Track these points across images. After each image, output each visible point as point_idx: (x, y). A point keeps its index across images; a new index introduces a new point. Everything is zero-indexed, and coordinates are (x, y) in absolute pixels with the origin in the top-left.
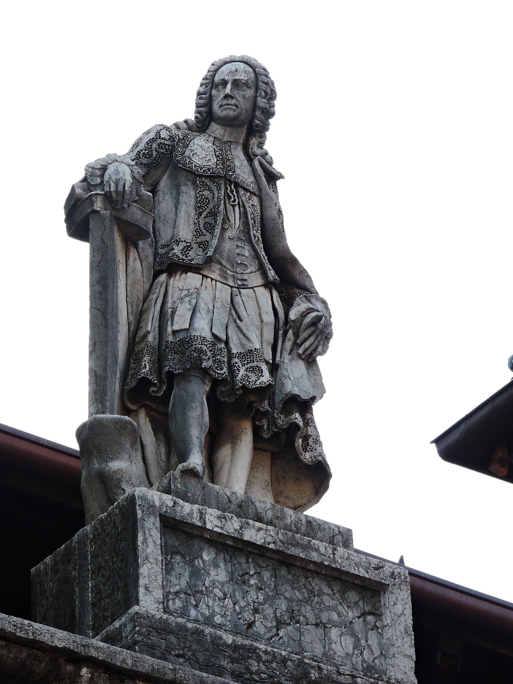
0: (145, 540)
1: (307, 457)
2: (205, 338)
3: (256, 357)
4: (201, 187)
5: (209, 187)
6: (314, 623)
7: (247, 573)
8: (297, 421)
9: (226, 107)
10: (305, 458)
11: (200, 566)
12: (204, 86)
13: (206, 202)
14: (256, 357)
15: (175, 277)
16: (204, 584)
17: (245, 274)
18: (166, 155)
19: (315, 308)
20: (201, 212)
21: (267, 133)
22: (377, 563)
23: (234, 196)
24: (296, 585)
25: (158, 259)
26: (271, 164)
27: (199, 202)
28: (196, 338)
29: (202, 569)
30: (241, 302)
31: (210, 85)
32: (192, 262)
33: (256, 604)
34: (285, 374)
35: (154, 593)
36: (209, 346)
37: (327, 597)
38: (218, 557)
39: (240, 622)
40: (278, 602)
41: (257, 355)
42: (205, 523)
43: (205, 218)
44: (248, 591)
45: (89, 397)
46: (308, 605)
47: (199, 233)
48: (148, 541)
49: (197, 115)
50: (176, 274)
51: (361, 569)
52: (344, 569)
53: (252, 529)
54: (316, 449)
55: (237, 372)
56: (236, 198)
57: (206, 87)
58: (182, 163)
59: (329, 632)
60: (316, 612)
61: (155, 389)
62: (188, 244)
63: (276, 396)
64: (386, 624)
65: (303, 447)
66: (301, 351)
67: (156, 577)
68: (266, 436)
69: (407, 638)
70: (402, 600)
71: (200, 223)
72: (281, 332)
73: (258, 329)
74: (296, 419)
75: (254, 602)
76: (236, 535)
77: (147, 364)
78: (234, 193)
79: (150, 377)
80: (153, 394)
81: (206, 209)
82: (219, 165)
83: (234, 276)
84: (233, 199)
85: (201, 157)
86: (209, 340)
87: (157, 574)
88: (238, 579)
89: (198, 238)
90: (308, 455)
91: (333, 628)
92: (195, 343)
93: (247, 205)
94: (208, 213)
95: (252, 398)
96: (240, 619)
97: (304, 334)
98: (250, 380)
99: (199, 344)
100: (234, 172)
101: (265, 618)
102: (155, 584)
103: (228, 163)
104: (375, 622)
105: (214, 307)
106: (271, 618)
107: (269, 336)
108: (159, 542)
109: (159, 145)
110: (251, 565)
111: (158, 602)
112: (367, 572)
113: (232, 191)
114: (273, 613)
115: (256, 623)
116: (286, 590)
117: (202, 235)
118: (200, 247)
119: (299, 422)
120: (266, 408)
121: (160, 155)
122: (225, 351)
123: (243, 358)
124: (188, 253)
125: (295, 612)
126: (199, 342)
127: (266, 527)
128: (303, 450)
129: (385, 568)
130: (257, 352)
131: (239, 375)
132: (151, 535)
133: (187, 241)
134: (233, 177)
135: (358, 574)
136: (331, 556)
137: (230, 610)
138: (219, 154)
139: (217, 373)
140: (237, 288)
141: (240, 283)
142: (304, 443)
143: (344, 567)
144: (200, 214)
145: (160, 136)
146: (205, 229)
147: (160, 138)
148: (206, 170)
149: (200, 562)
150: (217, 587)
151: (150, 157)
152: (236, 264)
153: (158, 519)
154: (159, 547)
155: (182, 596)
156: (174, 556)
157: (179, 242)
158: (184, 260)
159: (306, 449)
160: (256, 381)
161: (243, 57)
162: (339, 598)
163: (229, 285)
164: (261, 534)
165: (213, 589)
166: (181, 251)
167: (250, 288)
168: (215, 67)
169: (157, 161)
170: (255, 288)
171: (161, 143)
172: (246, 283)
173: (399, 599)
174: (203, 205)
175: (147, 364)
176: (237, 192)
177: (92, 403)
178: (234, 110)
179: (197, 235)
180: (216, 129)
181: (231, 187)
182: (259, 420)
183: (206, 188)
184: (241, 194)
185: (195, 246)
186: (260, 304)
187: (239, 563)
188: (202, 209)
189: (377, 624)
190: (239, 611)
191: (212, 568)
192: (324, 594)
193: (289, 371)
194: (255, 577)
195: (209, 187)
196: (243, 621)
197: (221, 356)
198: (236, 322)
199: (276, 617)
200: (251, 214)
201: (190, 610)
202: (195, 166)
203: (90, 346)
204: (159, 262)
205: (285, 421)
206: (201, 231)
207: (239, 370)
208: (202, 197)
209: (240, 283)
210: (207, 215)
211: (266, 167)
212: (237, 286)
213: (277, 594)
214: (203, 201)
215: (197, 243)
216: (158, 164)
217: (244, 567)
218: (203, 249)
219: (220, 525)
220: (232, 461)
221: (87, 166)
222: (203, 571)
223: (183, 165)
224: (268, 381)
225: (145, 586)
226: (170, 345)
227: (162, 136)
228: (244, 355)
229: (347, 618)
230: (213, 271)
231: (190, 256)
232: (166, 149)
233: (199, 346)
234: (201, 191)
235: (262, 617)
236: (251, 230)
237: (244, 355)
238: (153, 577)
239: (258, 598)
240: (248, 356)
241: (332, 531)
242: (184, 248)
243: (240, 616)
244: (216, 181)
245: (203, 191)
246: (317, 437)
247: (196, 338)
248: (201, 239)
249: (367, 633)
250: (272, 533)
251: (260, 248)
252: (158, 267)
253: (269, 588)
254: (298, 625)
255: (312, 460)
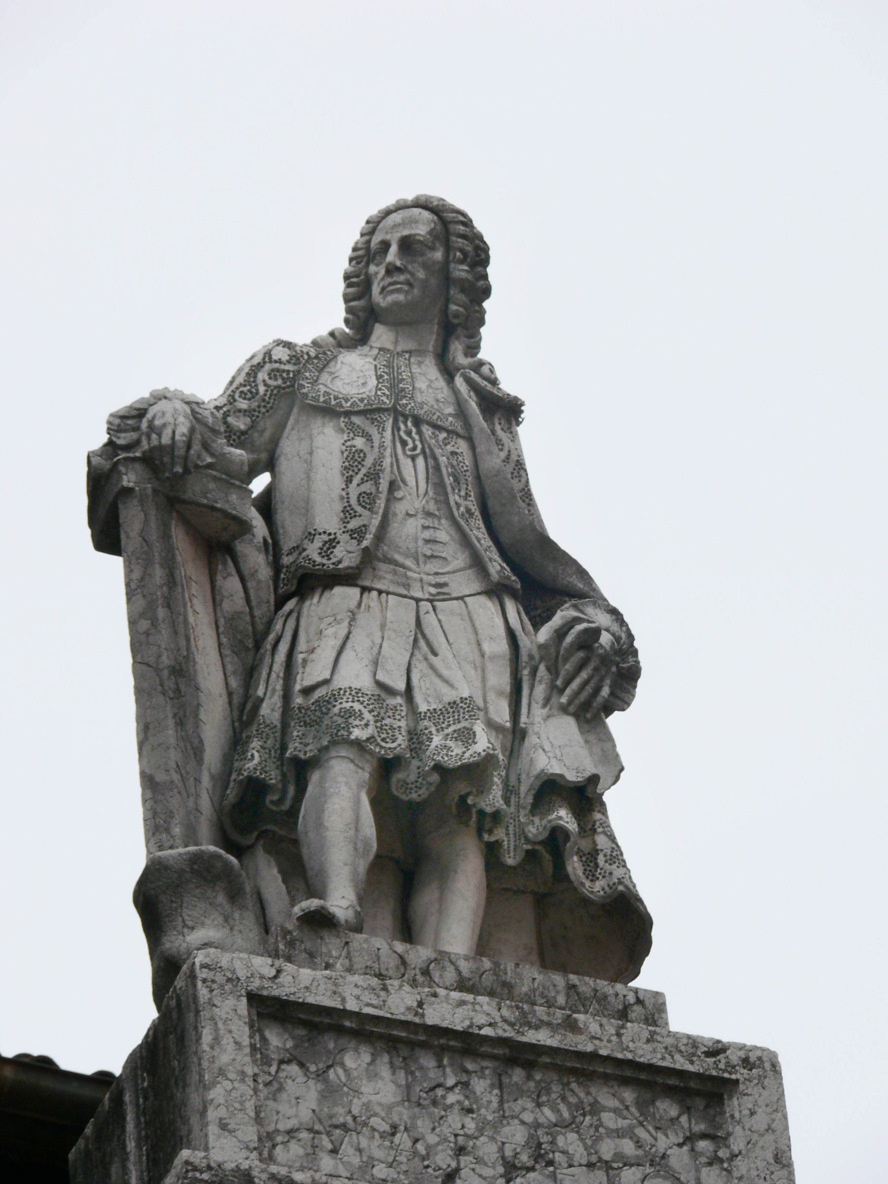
0: (217, 1040)
1: (597, 888)
2: (360, 690)
3: (464, 713)
4: (349, 433)
5: (363, 431)
6: (584, 1162)
7: (439, 1085)
8: (562, 822)
9: (391, 288)
10: (592, 892)
11: (340, 1080)
12: (354, 262)
13: (359, 457)
14: (464, 713)
15: (312, 598)
16: (350, 1112)
17: (443, 574)
18: (284, 388)
19: (582, 616)
20: (352, 476)
21: (483, 330)
22: (711, 1044)
23: (414, 441)
24: (544, 1098)
25: (282, 576)
26: (494, 382)
27: (346, 459)
28: (342, 692)
29: (345, 1085)
30: (436, 623)
31: (365, 259)
32: (340, 566)
33: (460, 1138)
34: (534, 743)
35: (239, 1134)
36: (367, 702)
37: (611, 1114)
38: (378, 1062)
39: (427, 1172)
40: (506, 1130)
41: (464, 709)
42: (344, 1000)
43: (358, 485)
44: (442, 1118)
45: (145, 825)
46: (572, 1131)
47: (350, 514)
48: (224, 1042)
49: (350, 316)
50: (313, 594)
51: (677, 1057)
52: (642, 1060)
53: (445, 1005)
54: (611, 874)
55: (428, 743)
56: (418, 443)
57: (358, 263)
58: (312, 397)
59: (618, 1175)
60: (589, 1142)
61: (275, 797)
62: (332, 537)
63: (522, 784)
64: (737, 1152)
65: (587, 872)
66: (564, 700)
67: (241, 1105)
68: (510, 861)
69: (779, 1172)
70: (767, 1105)
71: (351, 495)
72: (526, 672)
73: (475, 668)
74: (561, 818)
75: (456, 1135)
76: (410, 1017)
77: (256, 755)
78: (414, 434)
79: (261, 774)
80: (274, 808)
81: (359, 470)
82: (380, 389)
83: (421, 580)
84: (410, 445)
85: (347, 381)
86: (368, 693)
87: (244, 1098)
88: (420, 1098)
89: (348, 522)
90: (598, 885)
91: (625, 1168)
92: (340, 701)
93: (438, 452)
94: (365, 475)
95: (462, 788)
96: (427, 1167)
97: (567, 667)
98: (451, 754)
99: (347, 702)
100: (412, 398)
101: (479, 1160)
102: (240, 1115)
103: (401, 385)
104: (716, 1152)
105: (383, 638)
106: (493, 1160)
107: (500, 678)
108: (246, 1041)
109: (269, 374)
110: (448, 1070)
111: (247, 1148)
112: (692, 1062)
113: (409, 433)
114: (498, 1152)
115: (462, 1172)
116: (524, 1109)
117: (355, 516)
118: (352, 538)
119: (566, 825)
120: (497, 804)
121: (272, 391)
122: (402, 710)
123: (439, 719)
124: (332, 552)
125: (543, 1146)
126: (348, 698)
127: (474, 999)
128: (587, 878)
129: (728, 1052)
130: (466, 704)
131: (430, 748)
132: (230, 1032)
133: (328, 532)
134: (409, 407)
135: (672, 1066)
136: (614, 1038)
137: (405, 1153)
138: (383, 372)
139: (384, 748)
140: (428, 600)
141: (433, 590)
142: (588, 866)
143: (641, 1056)
144: (349, 480)
145: (270, 358)
146: (360, 504)
147: (270, 362)
148: (357, 401)
149: (340, 1071)
150: (375, 1115)
151: (253, 397)
152: (421, 559)
153: (244, 1000)
154: (247, 1050)
155: (304, 1135)
156: (283, 1067)
157: (315, 535)
158: (324, 565)
159: (594, 875)
160: (464, 753)
161: (417, 198)
162: (637, 1115)
163: (412, 598)
164: (461, 1012)
165: (369, 1119)
166: (319, 551)
167: (457, 599)
168: (371, 225)
169: (268, 403)
170: (467, 599)
171: (273, 370)
172: (445, 590)
173: (760, 1103)
174: (354, 463)
175: (256, 755)
176: (419, 433)
177: (151, 834)
178: (407, 292)
179: (346, 518)
180: (381, 335)
181: (406, 425)
182: (490, 832)
183: (359, 432)
184: (427, 436)
185: (344, 538)
186: (477, 624)
187: (421, 1068)
188: (353, 471)
189: (721, 1154)
190: (424, 1152)
191: (364, 1082)
192: (605, 1109)
193: (543, 736)
194: (457, 1090)
195: (363, 431)
196: (435, 1170)
197: (395, 719)
198: (426, 659)
199: (503, 1158)
200: (447, 467)
201: (321, 1159)
202: (336, 398)
203: (138, 734)
204: (284, 579)
205: (541, 826)
206: (352, 509)
207: (430, 740)
208: (351, 450)
209: (433, 590)
210: (362, 479)
211: (479, 384)
212: (427, 596)
213: (503, 1118)
214: (354, 456)
215: (347, 532)
216: (271, 408)
217: (432, 1075)
218: (358, 541)
219: (374, 1002)
220: (440, 912)
221: (112, 415)
222: (345, 1089)
223: (316, 399)
224: (484, 751)
225: (220, 1122)
226: (296, 714)
227: (274, 357)
228: (442, 713)
229: (654, 1150)
230: (380, 578)
231: (335, 556)
232: (283, 379)
233: (348, 705)
234: (349, 440)
235: (475, 1161)
236: (450, 496)
237: (442, 713)
238: (237, 1105)
239: (463, 1127)
240: (448, 713)
241: (622, 998)
242: (324, 545)
243: (426, 1163)
244: (376, 419)
245: (353, 439)
246: (612, 852)
247: (342, 692)
248: (353, 524)
249: (698, 1170)
250: (485, 1007)
251: (479, 533)
252: (283, 588)
253: (487, 1108)
254: (551, 1169)
255: (605, 893)
